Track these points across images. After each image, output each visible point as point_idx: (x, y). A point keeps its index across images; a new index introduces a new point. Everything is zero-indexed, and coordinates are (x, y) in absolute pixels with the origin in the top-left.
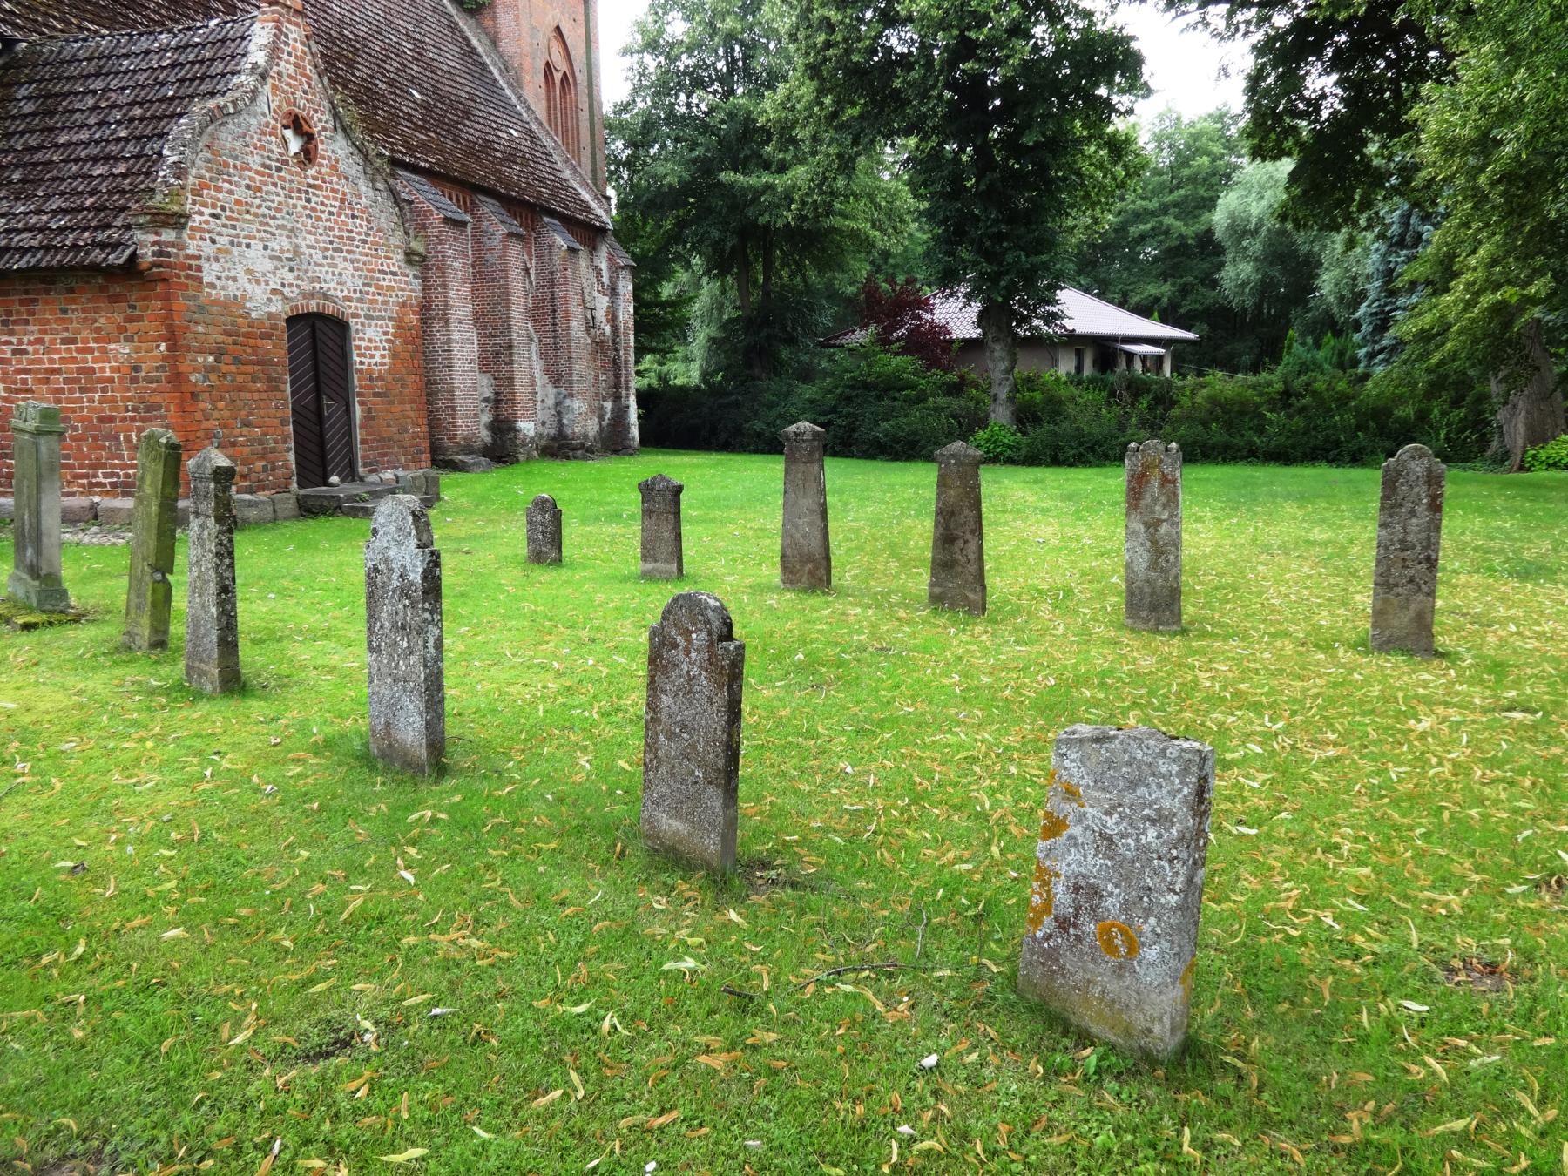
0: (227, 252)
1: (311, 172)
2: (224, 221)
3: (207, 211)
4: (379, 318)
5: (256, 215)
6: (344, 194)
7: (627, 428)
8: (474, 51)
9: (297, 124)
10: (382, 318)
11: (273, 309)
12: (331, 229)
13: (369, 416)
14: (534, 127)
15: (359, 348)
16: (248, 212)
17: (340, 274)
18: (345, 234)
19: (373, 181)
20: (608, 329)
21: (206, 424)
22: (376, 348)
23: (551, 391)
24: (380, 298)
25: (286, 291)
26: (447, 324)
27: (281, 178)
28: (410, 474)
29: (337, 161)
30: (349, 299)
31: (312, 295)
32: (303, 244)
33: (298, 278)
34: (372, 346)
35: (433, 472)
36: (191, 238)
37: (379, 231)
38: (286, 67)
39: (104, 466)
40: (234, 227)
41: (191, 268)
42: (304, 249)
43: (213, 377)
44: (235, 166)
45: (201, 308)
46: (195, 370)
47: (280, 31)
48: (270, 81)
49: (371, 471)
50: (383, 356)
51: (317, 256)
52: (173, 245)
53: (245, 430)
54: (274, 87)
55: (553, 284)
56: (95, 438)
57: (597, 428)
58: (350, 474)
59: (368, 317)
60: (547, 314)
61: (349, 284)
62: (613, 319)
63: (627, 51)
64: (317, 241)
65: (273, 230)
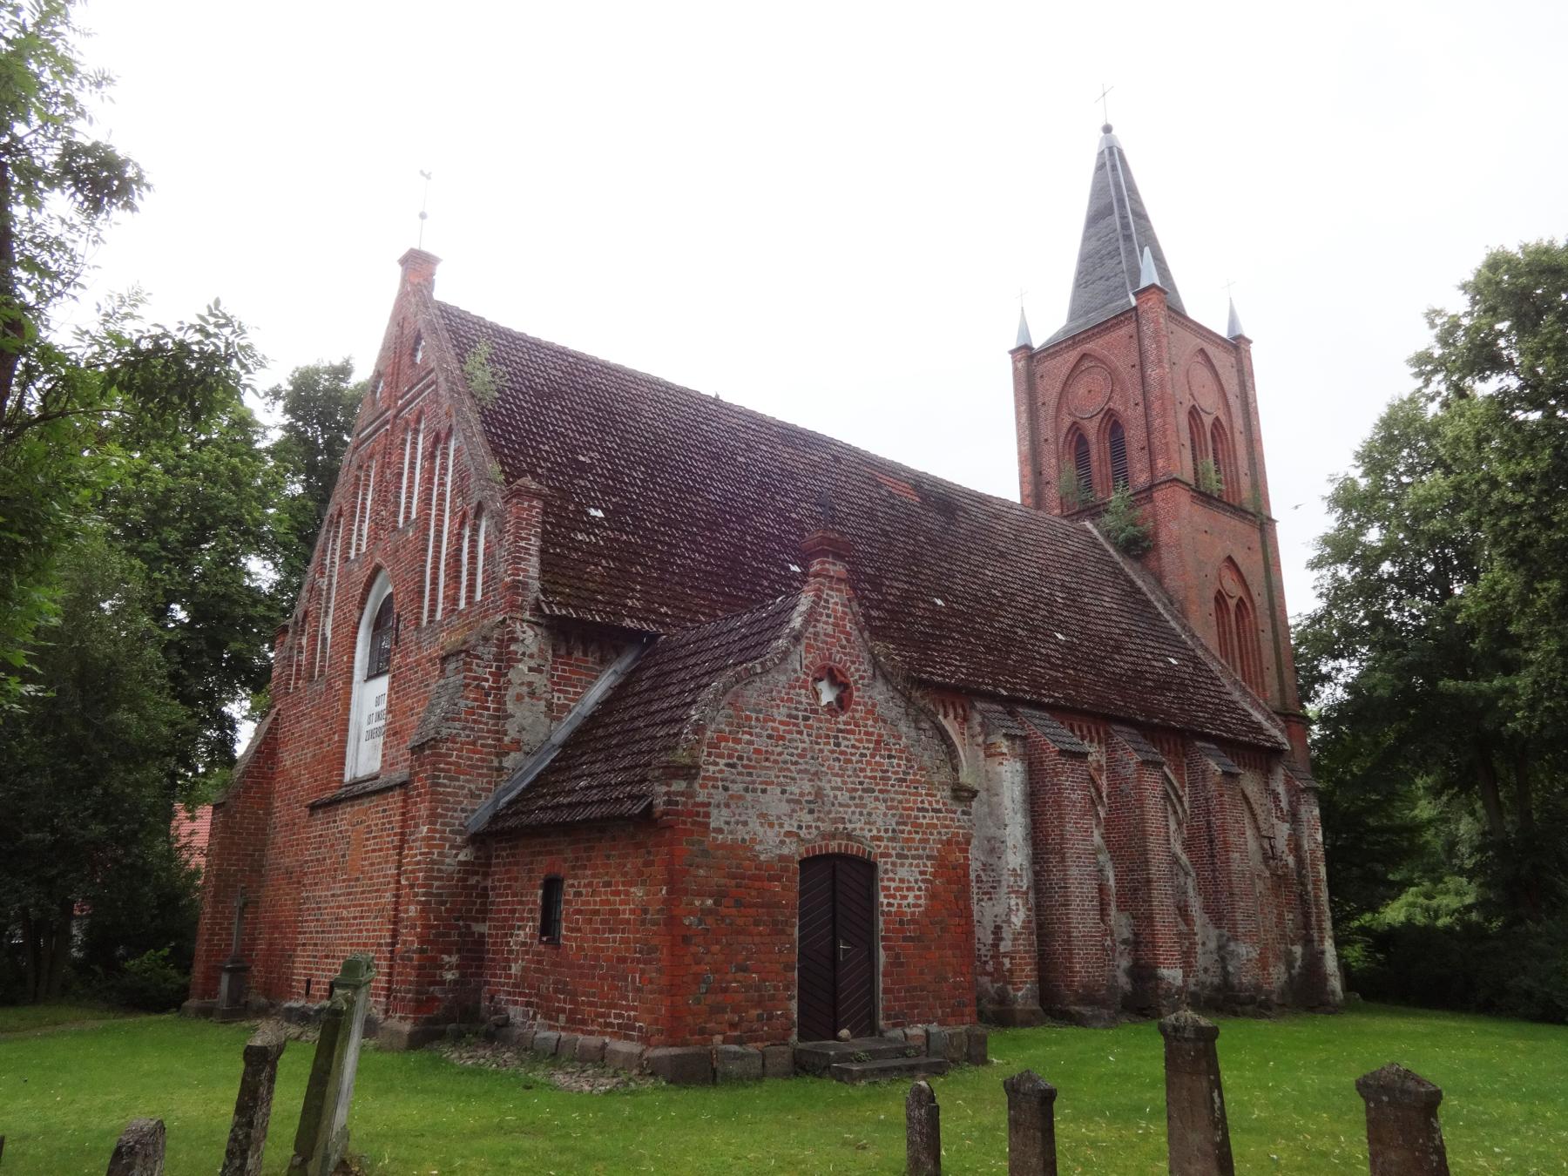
0: (741, 798)
1: (842, 718)
2: (740, 769)
3: (722, 762)
4: (914, 857)
5: (776, 762)
6: (880, 735)
7: (1323, 978)
8: (1139, 591)
9: (833, 676)
10: (920, 857)
11: (785, 851)
12: (862, 770)
13: (895, 962)
14: (1199, 653)
15: (888, 889)
16: (767, 760)
17: (870, 814)
18: (879, 774)
19: (916, 721)
20: (1291, 860)
21: (695, 968)
22: (909, 889)
23: (1213, 932)
24: (918, 837)
25: (803, 833)
26: (1063, 859)
27: (806, 726)
28: (947, 1030)
29: (874, 705)
30: (880, 839)
31: (833, 836)
32: (828, 786)
33: (818, 819)
34: (903, 889)
35: (980, 1030)
36: (702, 786)
37: (921, 769)
38: (824, 627)
39: (615, 1006)
40: (750, 774)
41: (698, 817)
42: (828, 791)
43: (710, 920)
44: (757, 719)
45: (705, 853)
46: (690, 913)
47: (819, 597)
48: (804, 641)
49: (895, 1025)
50: (918, 897)
51: (843, 797)
52: (682, 794)
53: (740, 976)
54: (809, 646)
55: (1208, 812)
56: (613, 978)
57: (1284, 977)
58: (866, 1026)
59: (899, 856)
60: (1206, 845)
61: (880, 823)
62: (1296, 848)
63: (1316, 564)
64: (844, 783)
65: (794, 775)
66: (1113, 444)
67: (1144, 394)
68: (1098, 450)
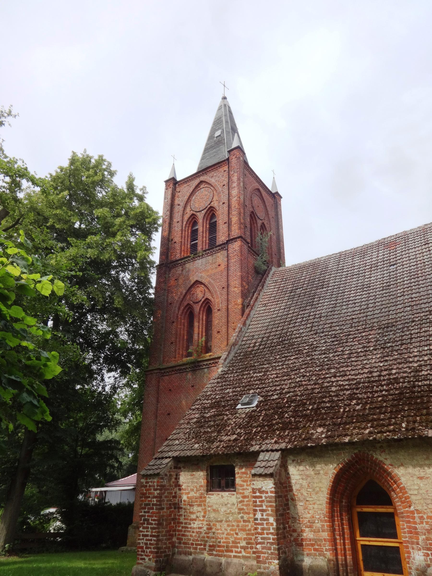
66: (210, 239)
67: (229, 200)
68: (202, 227)
